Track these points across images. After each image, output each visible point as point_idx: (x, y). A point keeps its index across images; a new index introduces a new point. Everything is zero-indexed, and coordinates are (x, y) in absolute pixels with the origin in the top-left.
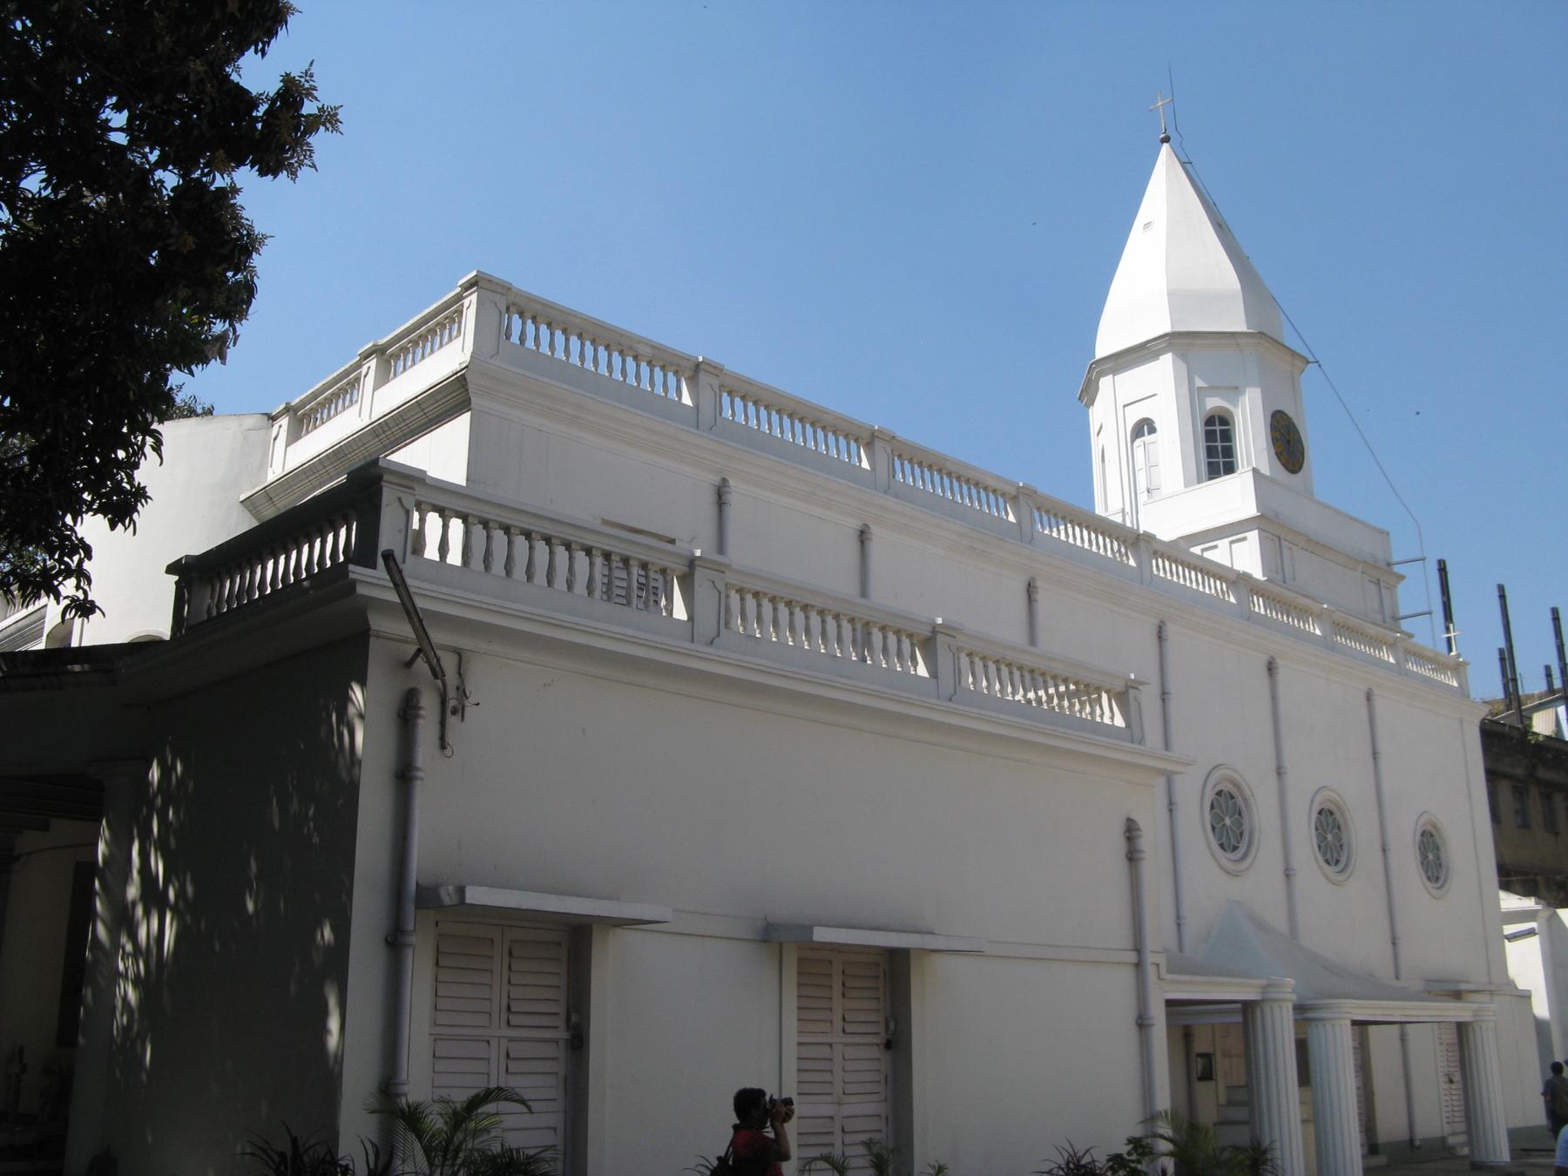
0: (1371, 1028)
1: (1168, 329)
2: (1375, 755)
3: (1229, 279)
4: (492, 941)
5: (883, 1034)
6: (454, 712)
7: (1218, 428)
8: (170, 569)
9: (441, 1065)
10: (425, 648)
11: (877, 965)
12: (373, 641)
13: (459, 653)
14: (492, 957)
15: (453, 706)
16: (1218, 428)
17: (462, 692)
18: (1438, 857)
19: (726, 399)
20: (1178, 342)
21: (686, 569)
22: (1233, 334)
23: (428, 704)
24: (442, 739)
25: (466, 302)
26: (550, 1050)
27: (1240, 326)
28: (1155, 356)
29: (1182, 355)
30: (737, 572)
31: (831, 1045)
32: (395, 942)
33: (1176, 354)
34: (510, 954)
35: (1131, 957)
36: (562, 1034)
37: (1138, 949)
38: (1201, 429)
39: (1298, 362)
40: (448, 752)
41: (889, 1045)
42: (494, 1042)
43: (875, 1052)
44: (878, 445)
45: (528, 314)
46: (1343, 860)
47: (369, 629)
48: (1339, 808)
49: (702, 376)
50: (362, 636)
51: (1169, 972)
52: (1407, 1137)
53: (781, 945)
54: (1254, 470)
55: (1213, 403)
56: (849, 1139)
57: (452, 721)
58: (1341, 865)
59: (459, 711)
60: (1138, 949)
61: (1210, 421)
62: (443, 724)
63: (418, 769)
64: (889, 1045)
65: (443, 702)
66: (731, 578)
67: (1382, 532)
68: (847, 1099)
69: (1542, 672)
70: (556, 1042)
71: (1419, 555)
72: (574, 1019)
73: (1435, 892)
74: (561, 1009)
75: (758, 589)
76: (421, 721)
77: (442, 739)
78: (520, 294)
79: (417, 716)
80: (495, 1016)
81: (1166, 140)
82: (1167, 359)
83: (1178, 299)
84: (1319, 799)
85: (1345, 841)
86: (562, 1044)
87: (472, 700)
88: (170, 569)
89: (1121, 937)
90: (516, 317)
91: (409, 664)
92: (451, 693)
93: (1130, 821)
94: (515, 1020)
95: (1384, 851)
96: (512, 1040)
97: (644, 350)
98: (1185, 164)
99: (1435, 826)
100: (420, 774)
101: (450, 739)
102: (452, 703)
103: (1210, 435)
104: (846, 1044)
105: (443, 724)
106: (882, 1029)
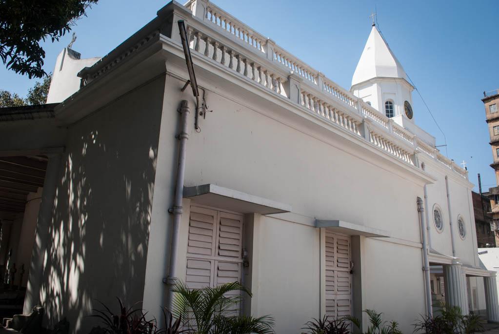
0: (471, 278)
1: (375, 76)
2: (448, 196)
3: (393, 63)
4: (213, 217)
5: (349, 268)
6: (201, 114)
7: (389, 105)
8: (79, 75)
9: (190, 272)
10: (192, 82)
11: (347, 241)
12: (167, 76)
13: (204, 90)
14: (212, 224)
15: (200, 112)
16: (389, 105)
17: (205, 106)
18: (462, 228)
19: (275, 55)
20: (378, 80)
21: (287, 79)
22: (394, 78)
23: (191, 108)
24: (196, 124)
25: (192, 4)
26: (235, 267)
27: (397, 76)
28: (372, 84)
29: (379, 85)
30: (305, 84)
31: (333, 271)
32: (173, 212)
33: (377, 84)
34: (220, 223)
35: (420, 246)
36: (240, 260)
37: (423, 243)
38: (385, 105)
39: (411, 88)
40: (198, 130)
41: (351, 272)
42: (213, 262)
43: (348, 275)
44: (320, 78)
45: (213, 12)
46: (440, 226)
47: (166, 70)
48: (440, 211)
49: (268, 44)
50: (162, 75)
51: (430, 252)
52: (343, 311)
53: (320, 228)
54: (402, 115)
55: (388, 98)
56: (340, 309)
57: (200, 118)
58: (440, 228)
59: (203, 114)
60: (423, 243)
61: (387, 103)
62: (196, 118)
63: (186, 134)
64: (351, 272)
65: (197, 109)
66: (302, 86)
67: (434, 137)
68: (339, 293)
69: (415, 200)
70: (237, 263)
71: (445, 144)
72: (245, 254)
73: (462, 238)
74: (239, 249)
75: (310, 93)
76: (188, 113)
77: (196, 124)
78: (212, 4)
79: (186, 111)
80: (213, 251)
81: (374, 25)
82: (375, 86)
83: (378, 68)
84: (434, 207)
85: (441, 221)
86: (240, 264)
87: (209, 109)
88: (79, 75)
89: (416, 238)
90: (209, 13)
91: (183, 89)
92: (200, 106)
93: (418, 197)
94: (222, 253)
95: (450, 224)
96: (220, 262)
97: (251, 32)
98: (380, 32)
99: (462, 218)
100: (187, 136)
101: (199, 125)
102: (200, 110)
103: (387, 107)
104: (338, 271)
105: (196, 118)
106: (348, 266)
